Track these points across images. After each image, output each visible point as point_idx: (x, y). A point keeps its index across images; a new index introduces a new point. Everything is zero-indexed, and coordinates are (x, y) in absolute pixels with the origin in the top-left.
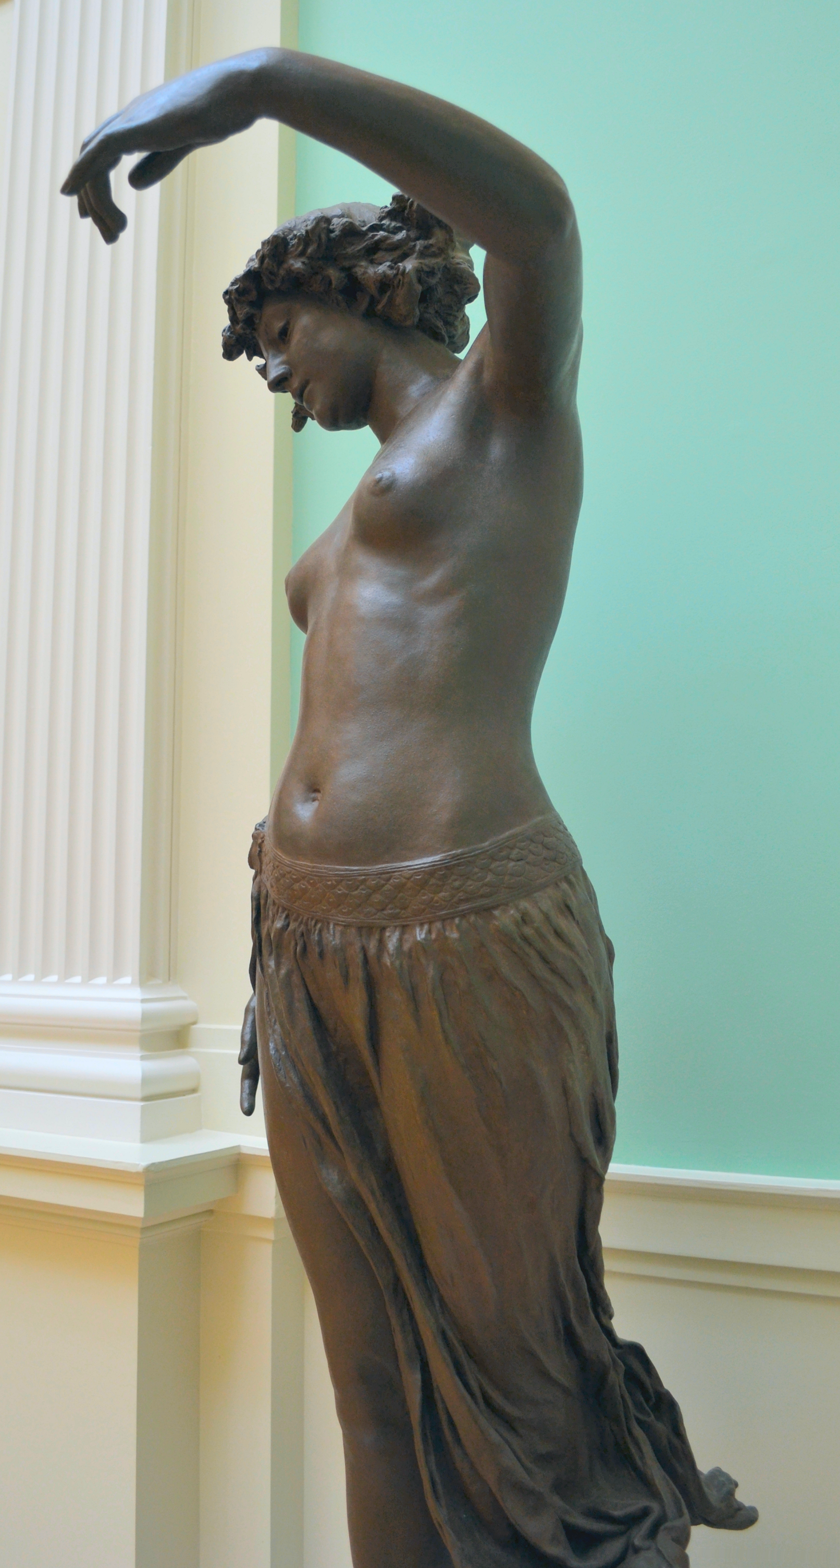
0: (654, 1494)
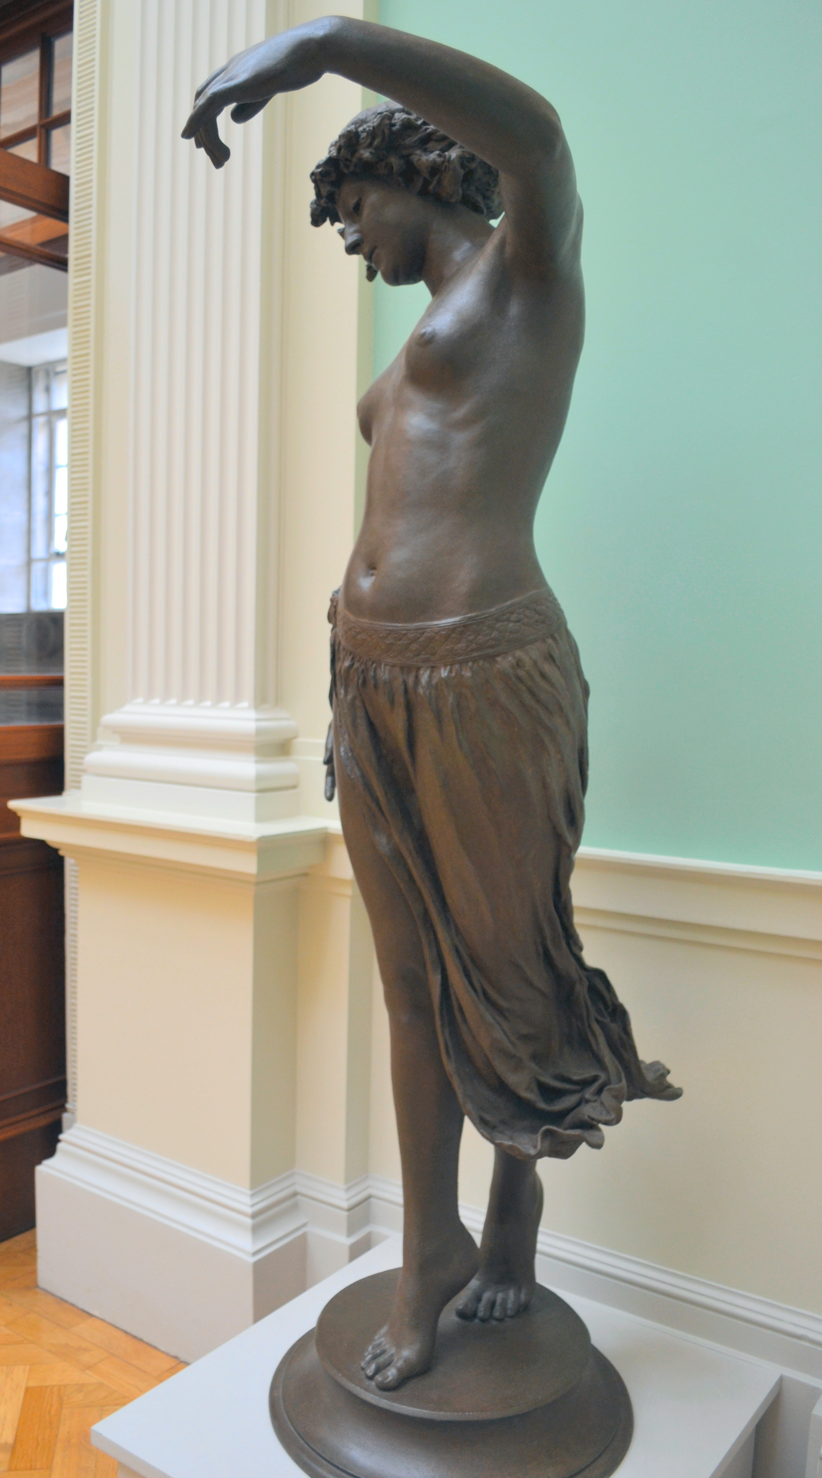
0: (599, 1061)
